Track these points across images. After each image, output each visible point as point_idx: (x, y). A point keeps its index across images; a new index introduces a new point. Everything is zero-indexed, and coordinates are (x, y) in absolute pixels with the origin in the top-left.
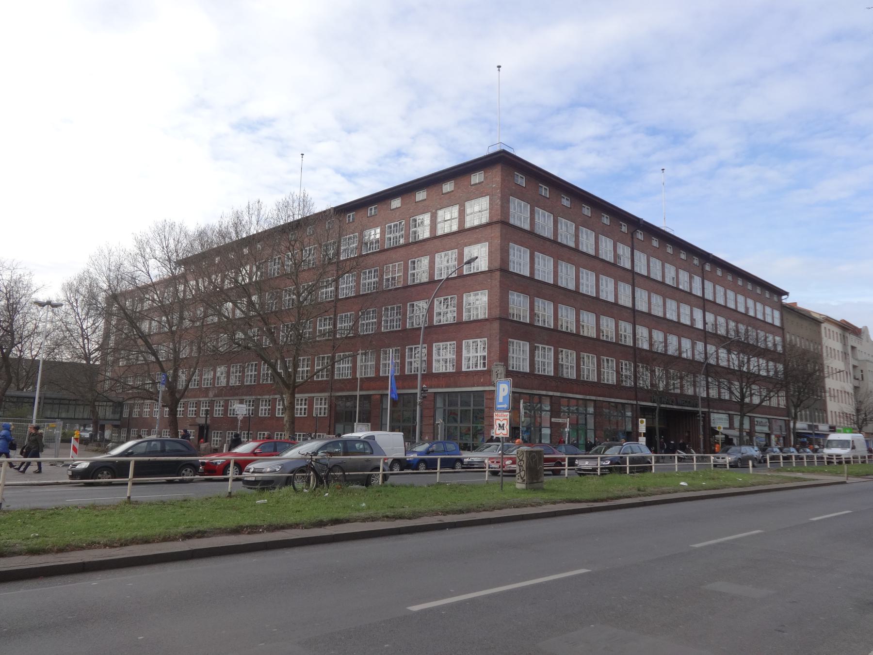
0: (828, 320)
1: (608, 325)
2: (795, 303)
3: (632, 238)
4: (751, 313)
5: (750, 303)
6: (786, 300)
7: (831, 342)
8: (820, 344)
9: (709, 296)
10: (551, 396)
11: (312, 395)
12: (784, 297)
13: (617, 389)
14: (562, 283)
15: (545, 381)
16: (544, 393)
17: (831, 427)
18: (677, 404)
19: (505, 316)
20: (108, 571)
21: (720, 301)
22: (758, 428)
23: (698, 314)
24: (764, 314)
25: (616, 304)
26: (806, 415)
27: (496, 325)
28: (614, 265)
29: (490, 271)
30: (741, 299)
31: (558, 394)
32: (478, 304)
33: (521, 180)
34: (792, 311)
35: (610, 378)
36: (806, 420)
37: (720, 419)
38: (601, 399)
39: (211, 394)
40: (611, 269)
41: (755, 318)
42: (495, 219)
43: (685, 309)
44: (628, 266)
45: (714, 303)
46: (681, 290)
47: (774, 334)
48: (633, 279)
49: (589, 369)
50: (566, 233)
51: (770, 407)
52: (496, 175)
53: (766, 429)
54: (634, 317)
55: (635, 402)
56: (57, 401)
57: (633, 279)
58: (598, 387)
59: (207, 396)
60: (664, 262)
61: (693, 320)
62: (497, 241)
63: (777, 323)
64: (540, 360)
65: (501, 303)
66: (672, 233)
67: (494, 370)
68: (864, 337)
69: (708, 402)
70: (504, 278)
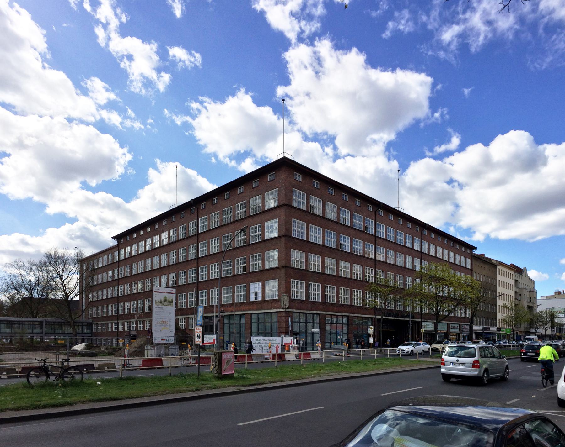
0: (501, 264)
1: (358, 269)
2: (484, 254)
3: (375, 214)
4: (464, 265)
5: (452, 254)
6: (477, 252)
7: (503, 279)
8: (496, 279)
9: (425, 251)
10: (320, 314)
11: (188, 316)
12: (474, 250)
13: (363, 309)
14: (398, 264)
15: (315, 305)
16: (315, 312)
17: (498, 329)
18: (401, 317)
19: (288, 265)
20: (145, 408)
21: (432, 253)
22: (452, 330)
23: (417, 262)
24: (460, 261)
25: (405, 268)
26: (480, 321)
27: (283, 271)
28: (385, 240)
29: (279, 237)
30: (446, 252)
31: (324, 313)
32: (273, 258)
33: (299, 178)
34: (481, 259)
35: (358, 302)
36: (480, 325)
37: (428, 325)
38: (352, 315)
39: (136, 317)
40: (362, 234)
41: (455, 264)
42: (282, 203)
43: (409, 259)
44: (372, 232)
45: (428, 255)
46: (407, 247)
47: (467, 273)
48: (375, 241)
49: (345, 297)
50: (331, 212)
51: (455, 317)
52: (283, 175)
53: (457, 331)
54: (375, 264)
55: (374, 316)
56: (81, 324)
57: (375, 241)
58: (350, 308)
59: (134, 318)
60: (396, 229)
61: (414, 266)
62: (283, 218)
63: (469, 267)
64: (313, 292)
65: (285, 258)
66: (402, 211)
67: (282, 299)
68: (524, 274)
69: (422, 315)
70: (287, 240)
